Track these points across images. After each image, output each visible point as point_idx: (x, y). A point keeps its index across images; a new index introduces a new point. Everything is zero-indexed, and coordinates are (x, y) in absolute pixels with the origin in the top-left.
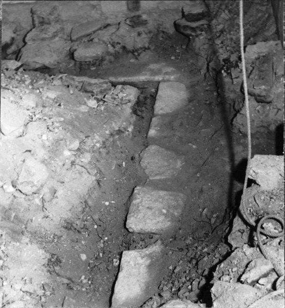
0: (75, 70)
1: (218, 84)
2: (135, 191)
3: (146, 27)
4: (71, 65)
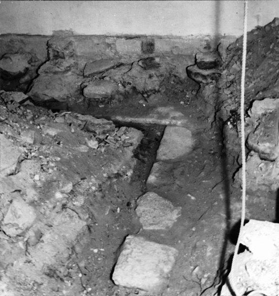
0: (84, 105)
1: (222, 136)
2: (127, 241)
3: (157, 71)
4: (80, 100)
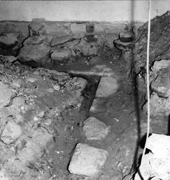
0: (51, 64)
1: (135, 83)
2: (77, 146)
3: (96, 43)
4: (49, 61)
